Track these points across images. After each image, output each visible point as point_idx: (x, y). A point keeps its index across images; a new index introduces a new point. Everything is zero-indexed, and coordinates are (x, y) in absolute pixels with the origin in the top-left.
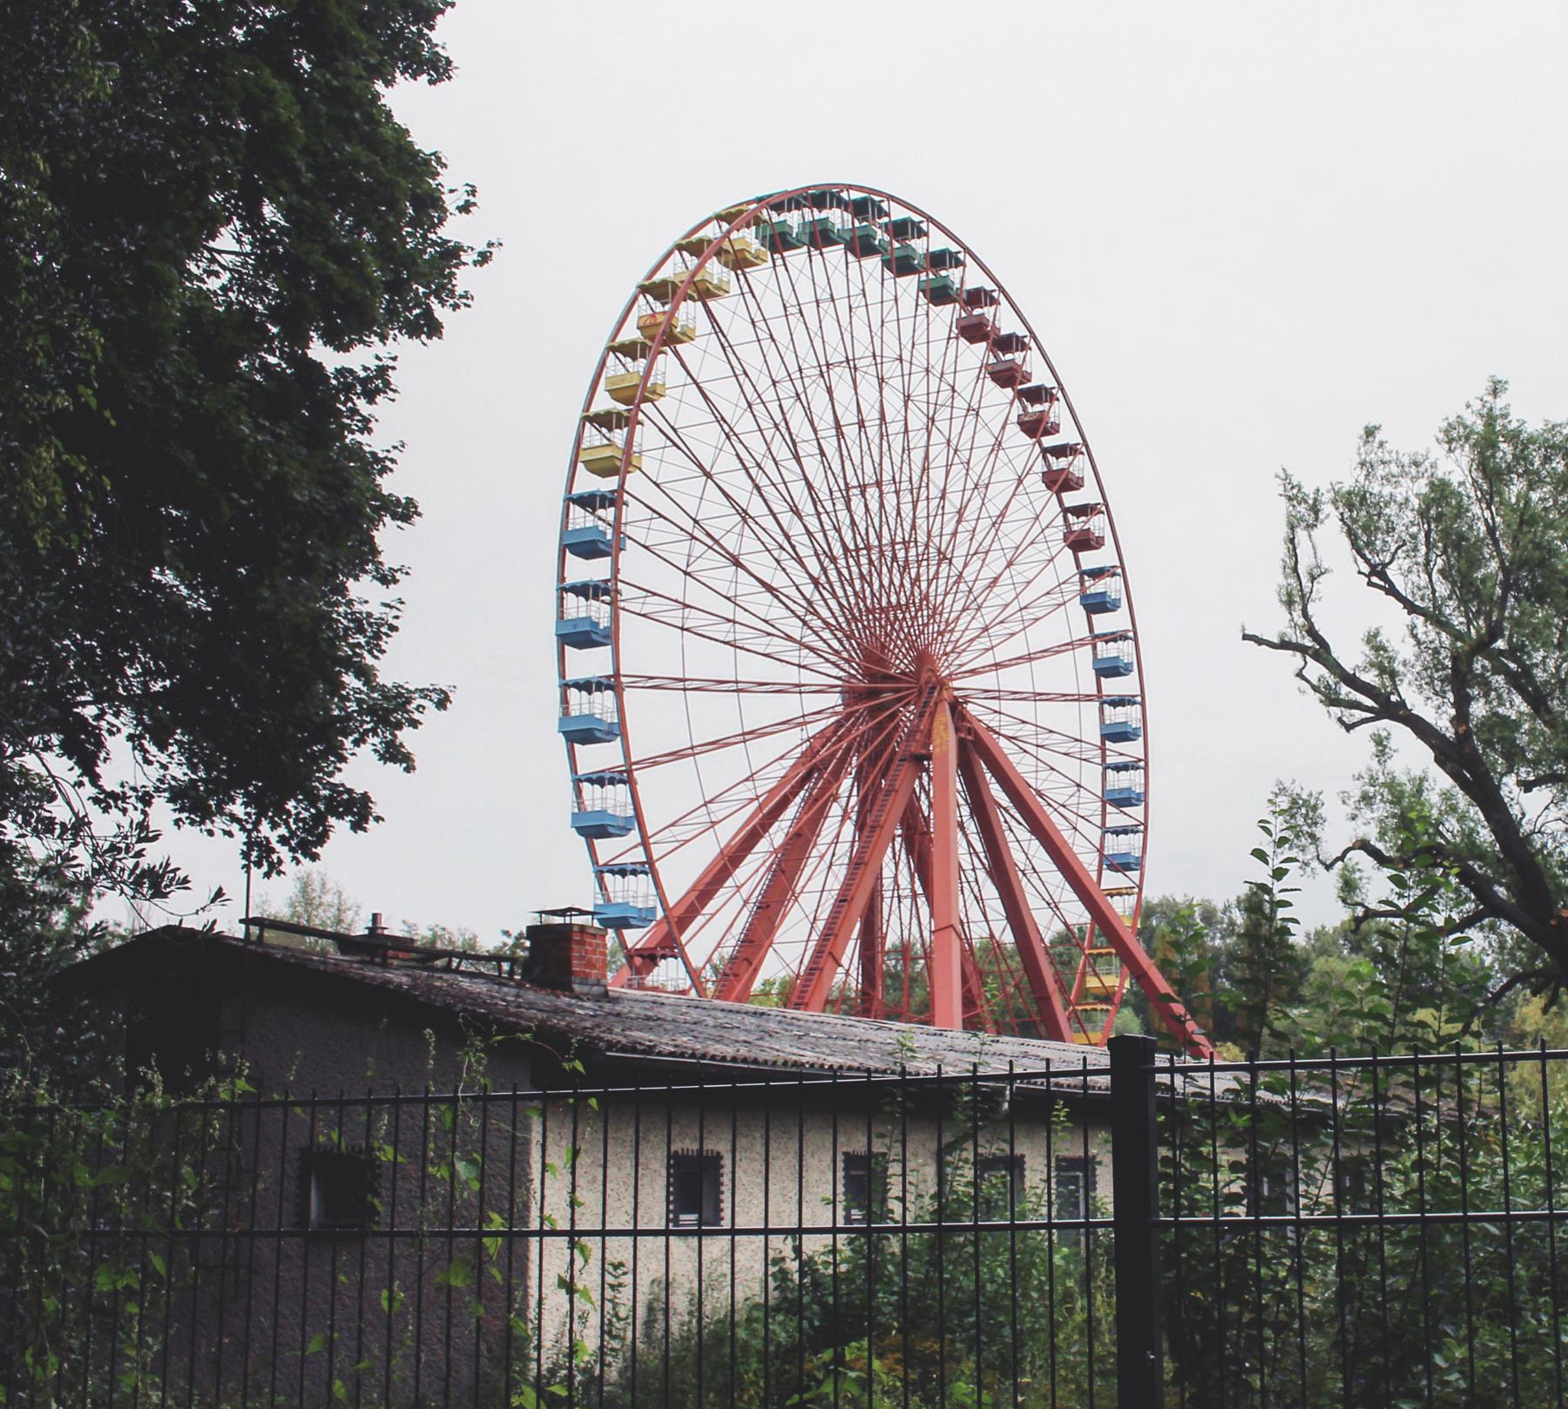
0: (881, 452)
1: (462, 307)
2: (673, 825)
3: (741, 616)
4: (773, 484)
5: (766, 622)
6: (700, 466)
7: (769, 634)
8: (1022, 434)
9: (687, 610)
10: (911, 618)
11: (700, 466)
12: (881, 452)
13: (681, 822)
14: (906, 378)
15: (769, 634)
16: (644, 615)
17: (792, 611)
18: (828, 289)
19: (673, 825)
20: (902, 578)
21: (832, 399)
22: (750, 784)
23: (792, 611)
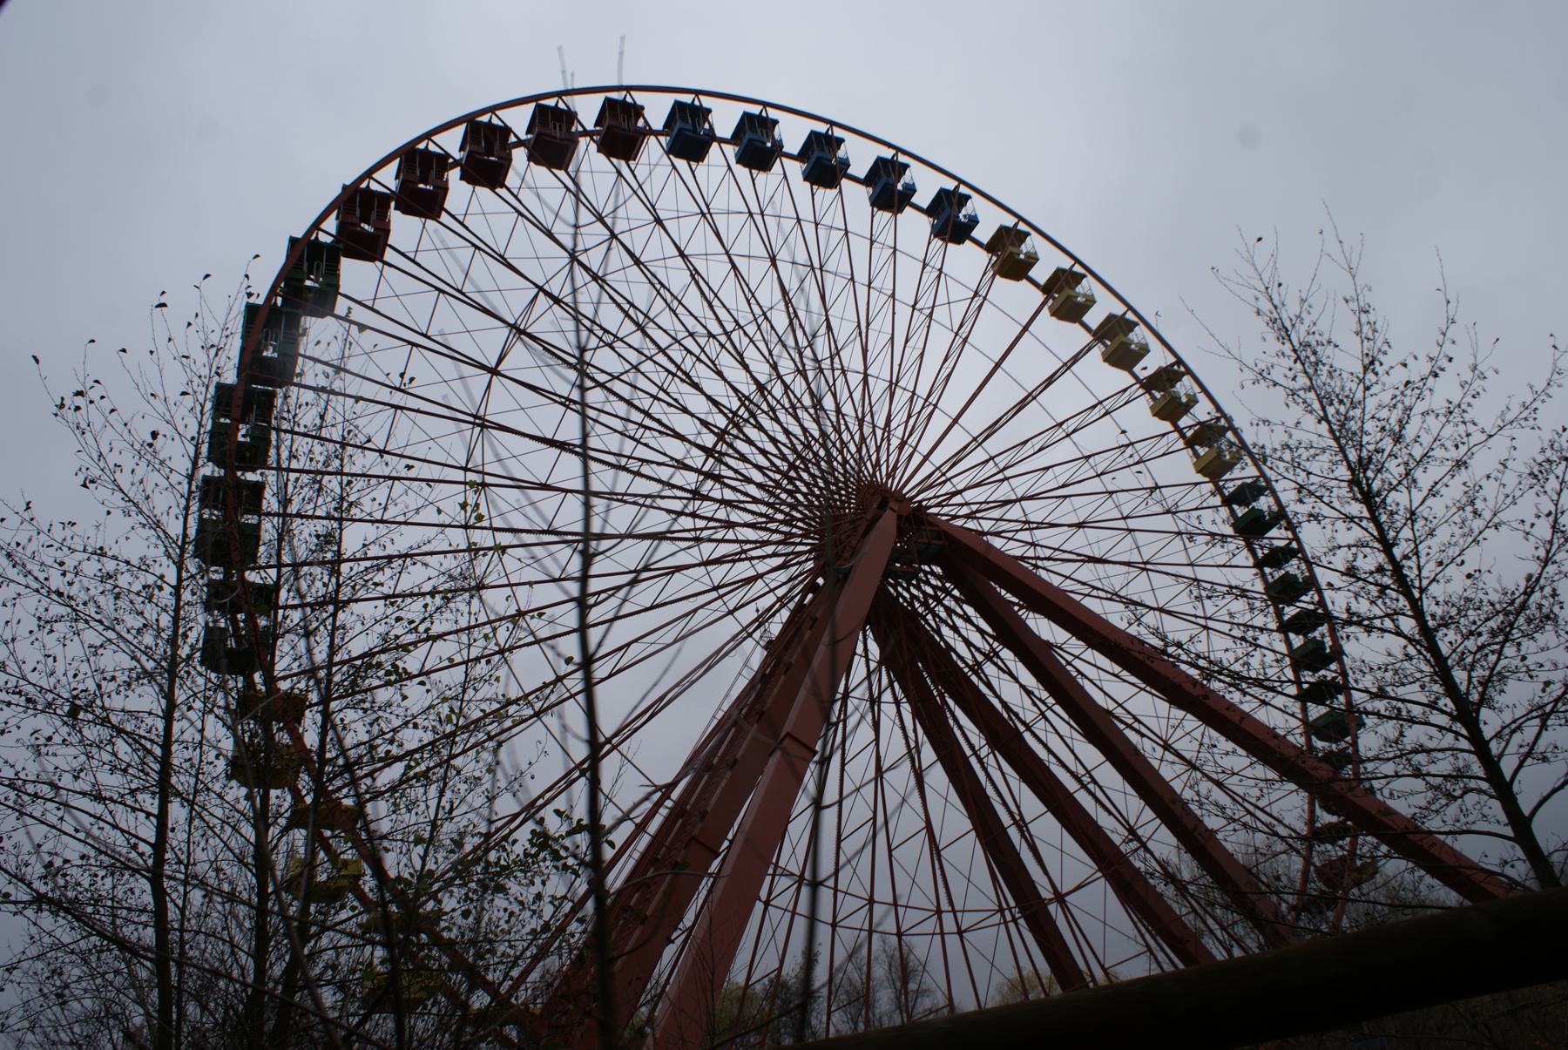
0: (1003, 774)
1: (419, 564)
2: (922, 355)
3: (1095, 485)
4: (1077, 657)
5: (1066, 497)
6: (1169, 613)
7: (1064, 486)
8: (828, 191)
9: (1091, 460)
10: (847, 462)
11: (1169, 613)
12: (1003, 774)
13: (918, 361)
14: (640, 192)
15: (1064, 486)
16: (1047, 468)
17: (1064, 551)
18: (660, 369)
19: (922, 355)
20: (796, 418)
21: (692, 415)
22: (928, 269)
23: (1064, 551)
